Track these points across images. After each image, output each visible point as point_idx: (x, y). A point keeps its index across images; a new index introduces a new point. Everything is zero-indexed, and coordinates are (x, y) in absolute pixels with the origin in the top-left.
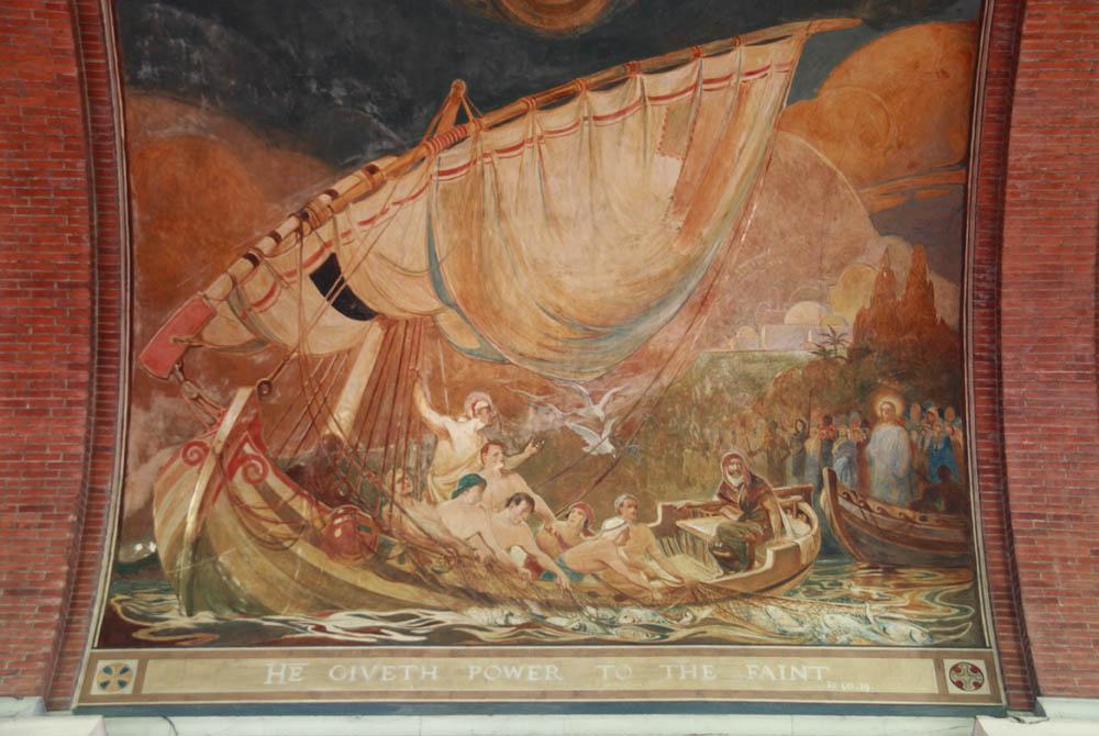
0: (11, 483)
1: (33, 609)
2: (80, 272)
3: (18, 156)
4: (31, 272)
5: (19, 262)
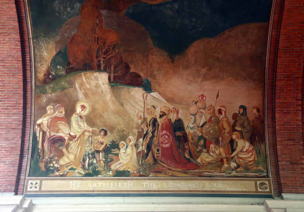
0: (283, 133)
1: (299, 168)
2: (299, 74)
3: (287, 42)
4: (286, 74)
5: (283, 71)
